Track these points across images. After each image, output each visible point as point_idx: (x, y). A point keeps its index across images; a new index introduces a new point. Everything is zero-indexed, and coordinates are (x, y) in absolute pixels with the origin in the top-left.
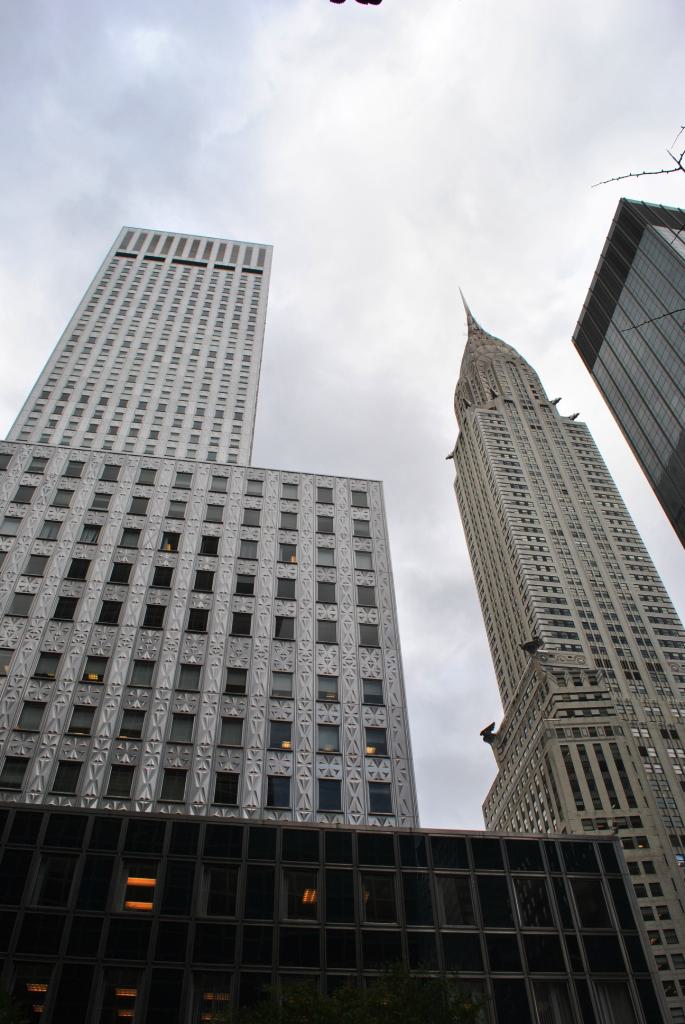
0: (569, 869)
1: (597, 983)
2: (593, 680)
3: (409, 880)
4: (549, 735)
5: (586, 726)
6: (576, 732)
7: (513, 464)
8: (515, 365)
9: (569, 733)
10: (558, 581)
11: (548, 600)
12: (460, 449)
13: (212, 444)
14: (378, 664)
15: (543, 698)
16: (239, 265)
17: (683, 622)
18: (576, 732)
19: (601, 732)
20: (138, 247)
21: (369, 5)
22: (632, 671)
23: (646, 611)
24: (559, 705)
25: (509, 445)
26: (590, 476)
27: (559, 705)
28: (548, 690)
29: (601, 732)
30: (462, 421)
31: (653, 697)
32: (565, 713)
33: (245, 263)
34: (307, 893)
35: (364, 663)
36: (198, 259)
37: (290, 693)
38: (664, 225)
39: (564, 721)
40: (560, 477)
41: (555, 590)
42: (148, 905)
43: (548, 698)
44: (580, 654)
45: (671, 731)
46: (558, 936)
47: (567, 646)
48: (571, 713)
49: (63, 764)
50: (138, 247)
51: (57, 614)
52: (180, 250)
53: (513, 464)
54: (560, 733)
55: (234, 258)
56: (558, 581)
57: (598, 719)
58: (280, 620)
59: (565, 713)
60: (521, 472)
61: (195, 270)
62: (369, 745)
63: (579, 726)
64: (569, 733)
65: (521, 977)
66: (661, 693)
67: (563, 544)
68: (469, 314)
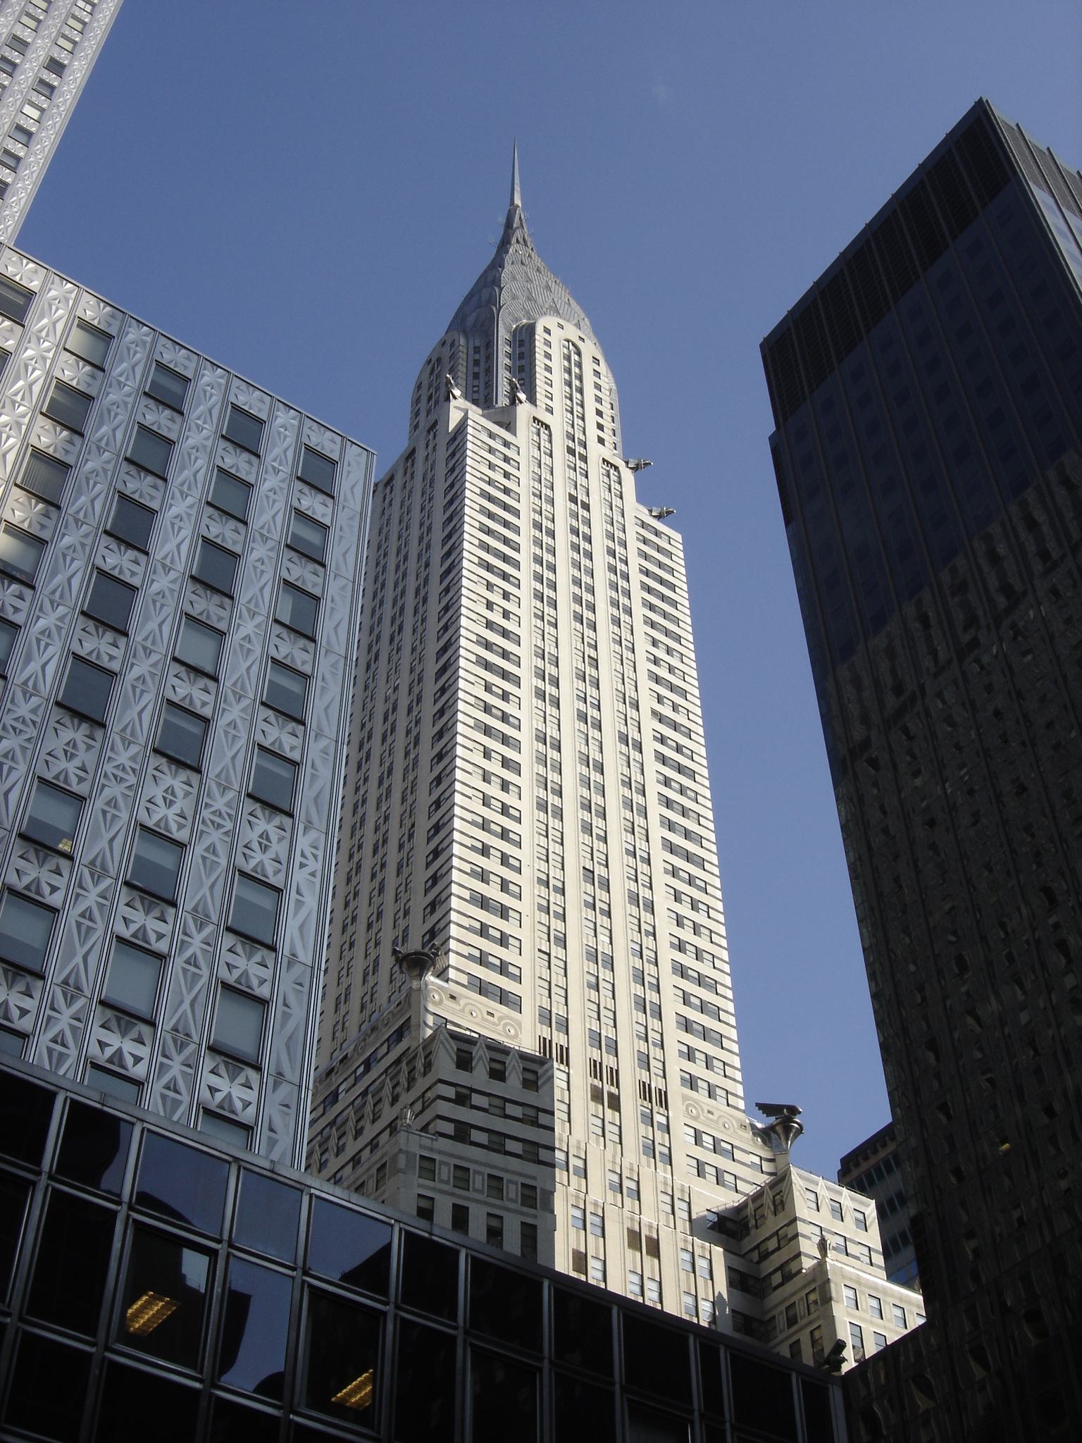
2: (530, 1076)
4: (402, 1162)
5: (488, 1171)
6: (462, 1175)
7: (505, 633)
8: (579, 353)
9: (445, 1173)
10: (519, 845)
11: (490, 625)
12: (398, 482)
14: (89, 758)
15: (411, 1080)
18: (462, 1175)
19: (512, 1191)
21: (184, 1271)
22: (607, 1088)
23: (666, 871)
24: (444, 1108)
25: (510, 799)
26: (659, 708)
27: (444, 1108)
28: (428, 1066)
29: (512, 1191)
30: (424, 425)
31: (633, 1155)
32: (449, 1128)
39: (443, 1144)
40: (600, 769)
41: (504, 885)
43: (421, 1084)
44: (515, 1014)
45: (649, 1239)
47: (492, 932)
48: (462, 1132)
53: (505, 633)
54: (428, 1166)
56: (519, 845)
57: (514, 1163)
59: (449, 1128)
60: (517, 746)
63: (472, 1167)
64: (445, 1173)
66: (650, 1150)
67: (556, 889)
68: (498, 263)
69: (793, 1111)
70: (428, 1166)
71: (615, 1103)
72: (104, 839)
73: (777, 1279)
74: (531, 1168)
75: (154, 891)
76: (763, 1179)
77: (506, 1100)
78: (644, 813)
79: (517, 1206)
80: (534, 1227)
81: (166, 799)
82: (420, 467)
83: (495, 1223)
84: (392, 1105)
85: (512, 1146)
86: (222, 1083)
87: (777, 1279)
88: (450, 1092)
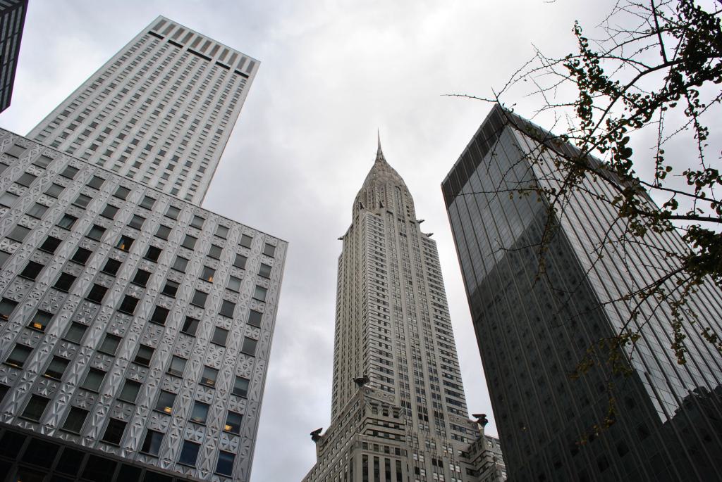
2: (386, 412)
4: (357, 445)
5: (373, 443)
9: (371, 447)
12: (349, 235)
16: (234, 67)
18: (376, 447)
19: (392, 451)
20: (166, 32)
24: (369, 426)
27: (369, 426)
28: (364, 414)
29: (392, 451)
31: (433, 435)
35: (240, 365)
36: (207, 54)
48: (375, 433)
50: (166, 32)
51: (75, 258)
54: (365, 445)
55: (231, 61)
57: (392, 442)
59: (371, 433)
62: (228, 424)
63: (390, 446)
66: (439, 433)
69: (484, 416)
70: (365, 445)
71: (426, 419)
72: (194, 372)
73: (481, 470)
74: (398, 443)
75: (207, 384)
76: (476, 438)
77: (378, 420)
78: (430, 327)
79: (383, 453)
80: (400, 462)
81: (214, 356)
82: (355, 230)
83: (376, 459)
84: (321, 429)
85: (391, 436)
86: (192, 432)
87: (481, 470)
88: (371, 421)
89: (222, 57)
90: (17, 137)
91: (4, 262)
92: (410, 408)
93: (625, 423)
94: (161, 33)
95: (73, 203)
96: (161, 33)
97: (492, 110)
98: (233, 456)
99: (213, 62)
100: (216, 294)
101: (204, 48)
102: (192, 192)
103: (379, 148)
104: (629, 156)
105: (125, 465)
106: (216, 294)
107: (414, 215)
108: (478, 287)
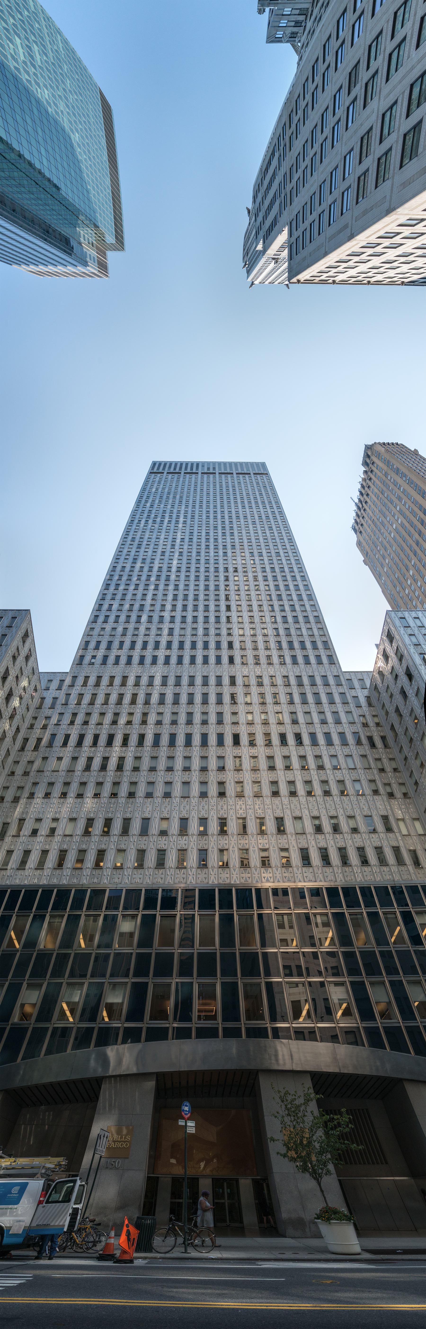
0: (267, 1028)
1: (408, 982)
3: (260, 916)
5: (390, 813)
13: (205, 600)
16: (217, 471)
17: (425, 1133)
20: (164, 469)
22: (345, 910)
33: (216, 1036)
34: (234, 1051)
35: (234, 670)
36: (194, 471)
37: (207, 767)
38: (290, 234)
42: (83, 945)
46: (133, 983)
49: (125, 819)
50: (164, 469)
51: (123, 833)
52: (186, 469)
55: (181, 468)
58: (227, 572)
61: (194, 475)
62: (200, 826)
65: (333, 1025)
89: (186, 469)
90: (272, 19)
91: (398, 207)
92: (198, 1036)
93: (315, 1274)
94: (157, 469)
95: (92, 268)
96: (157, 469)
97: (265, 1129)
98: (225, 819)
99: (182, 473)
100: (151, 640)
101: (192, 469)
102: (216, 558)
103: (319, 1184)
104: (416, 452)
105: (186, 890)
106: (151, 640)
107: (332, 660)
108: (30, 1226)
